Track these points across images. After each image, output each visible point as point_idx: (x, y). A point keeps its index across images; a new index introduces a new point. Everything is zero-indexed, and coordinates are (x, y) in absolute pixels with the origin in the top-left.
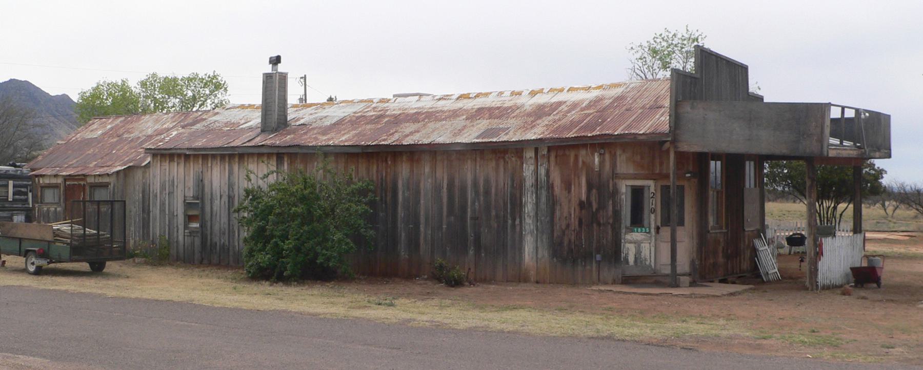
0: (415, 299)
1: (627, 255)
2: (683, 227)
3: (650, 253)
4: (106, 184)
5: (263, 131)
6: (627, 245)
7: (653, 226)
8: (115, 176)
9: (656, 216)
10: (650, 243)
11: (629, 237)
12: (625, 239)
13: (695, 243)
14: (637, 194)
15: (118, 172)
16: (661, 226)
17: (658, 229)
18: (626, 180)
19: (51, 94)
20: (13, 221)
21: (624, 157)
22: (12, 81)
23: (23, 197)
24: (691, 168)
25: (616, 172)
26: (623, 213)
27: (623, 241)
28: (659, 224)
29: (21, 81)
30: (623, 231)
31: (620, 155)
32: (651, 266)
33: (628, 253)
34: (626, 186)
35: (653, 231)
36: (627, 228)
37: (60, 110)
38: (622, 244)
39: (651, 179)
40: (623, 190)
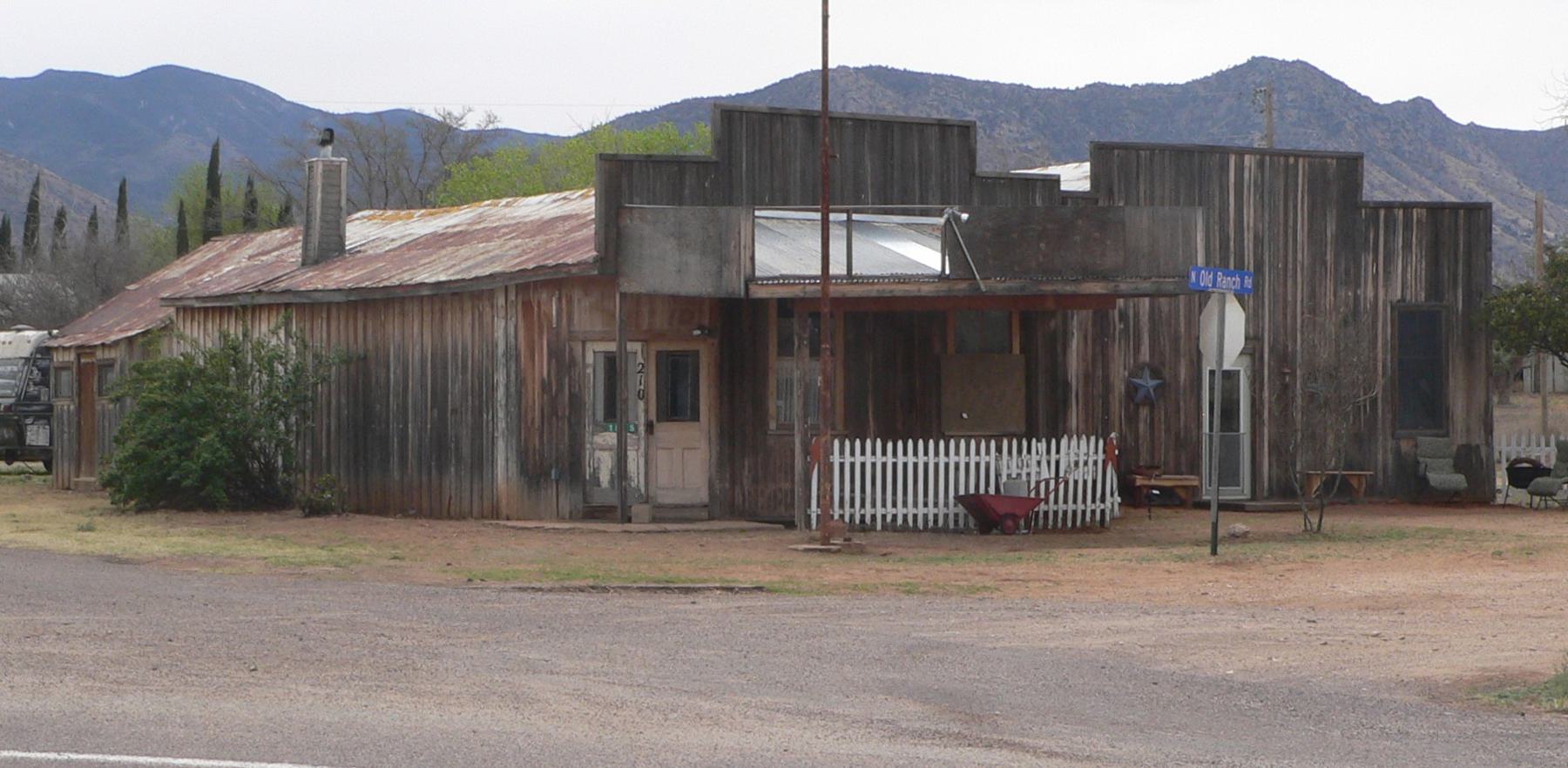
0: (1302, 677)
1: (596, 471)
2: (697, 423)
3: (638, 468)
4: (111, 362)
5: (304, 264)
6: (598, 454)
7: (642, 420)
8: (123, 346)
9: (647, 404)
10: (637, 450)
11: (598, 439)
12: (591, 443)
13: (714, 452)
14: (613, 367)
15: (130, 340)
16: (658, 421)
17: (650, 427)
18: (595, 344)
19: (1375, 100)
20: (599, 485)
21: (586, 303)
22: (1256, 64)
23: (787, 432)
24: (706, 322)
25: (572, 329)
26: (588, 399)
27: (588, 446)
28: (653, 417)
29: (1284, 63)
30: (589, 429)
31: (579, 300)
32: (640, 490)
33: (598, 468)
34: (594, 352)
35: (642, 429)
36: (595, 423)
37: (1406, 148)
38: (588, 452)
39: (638, 341)
40: (590, 359)
